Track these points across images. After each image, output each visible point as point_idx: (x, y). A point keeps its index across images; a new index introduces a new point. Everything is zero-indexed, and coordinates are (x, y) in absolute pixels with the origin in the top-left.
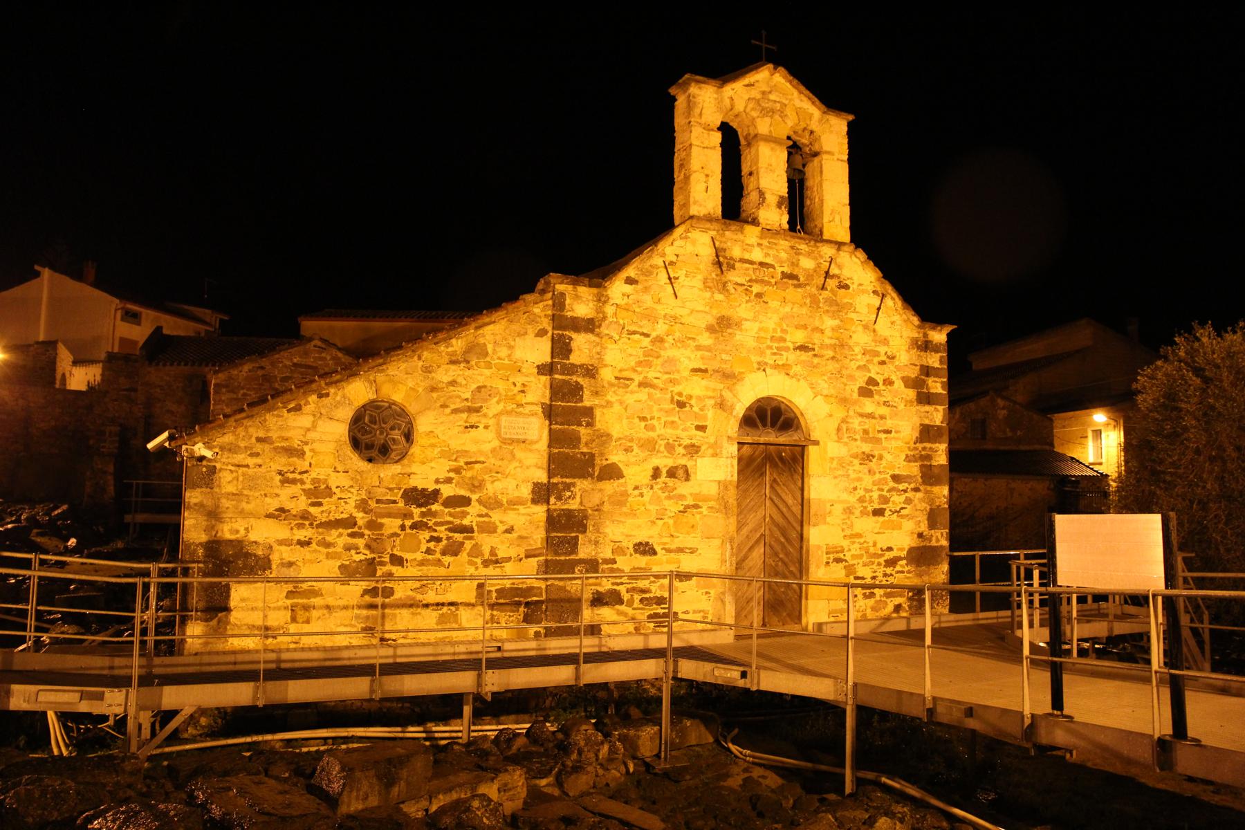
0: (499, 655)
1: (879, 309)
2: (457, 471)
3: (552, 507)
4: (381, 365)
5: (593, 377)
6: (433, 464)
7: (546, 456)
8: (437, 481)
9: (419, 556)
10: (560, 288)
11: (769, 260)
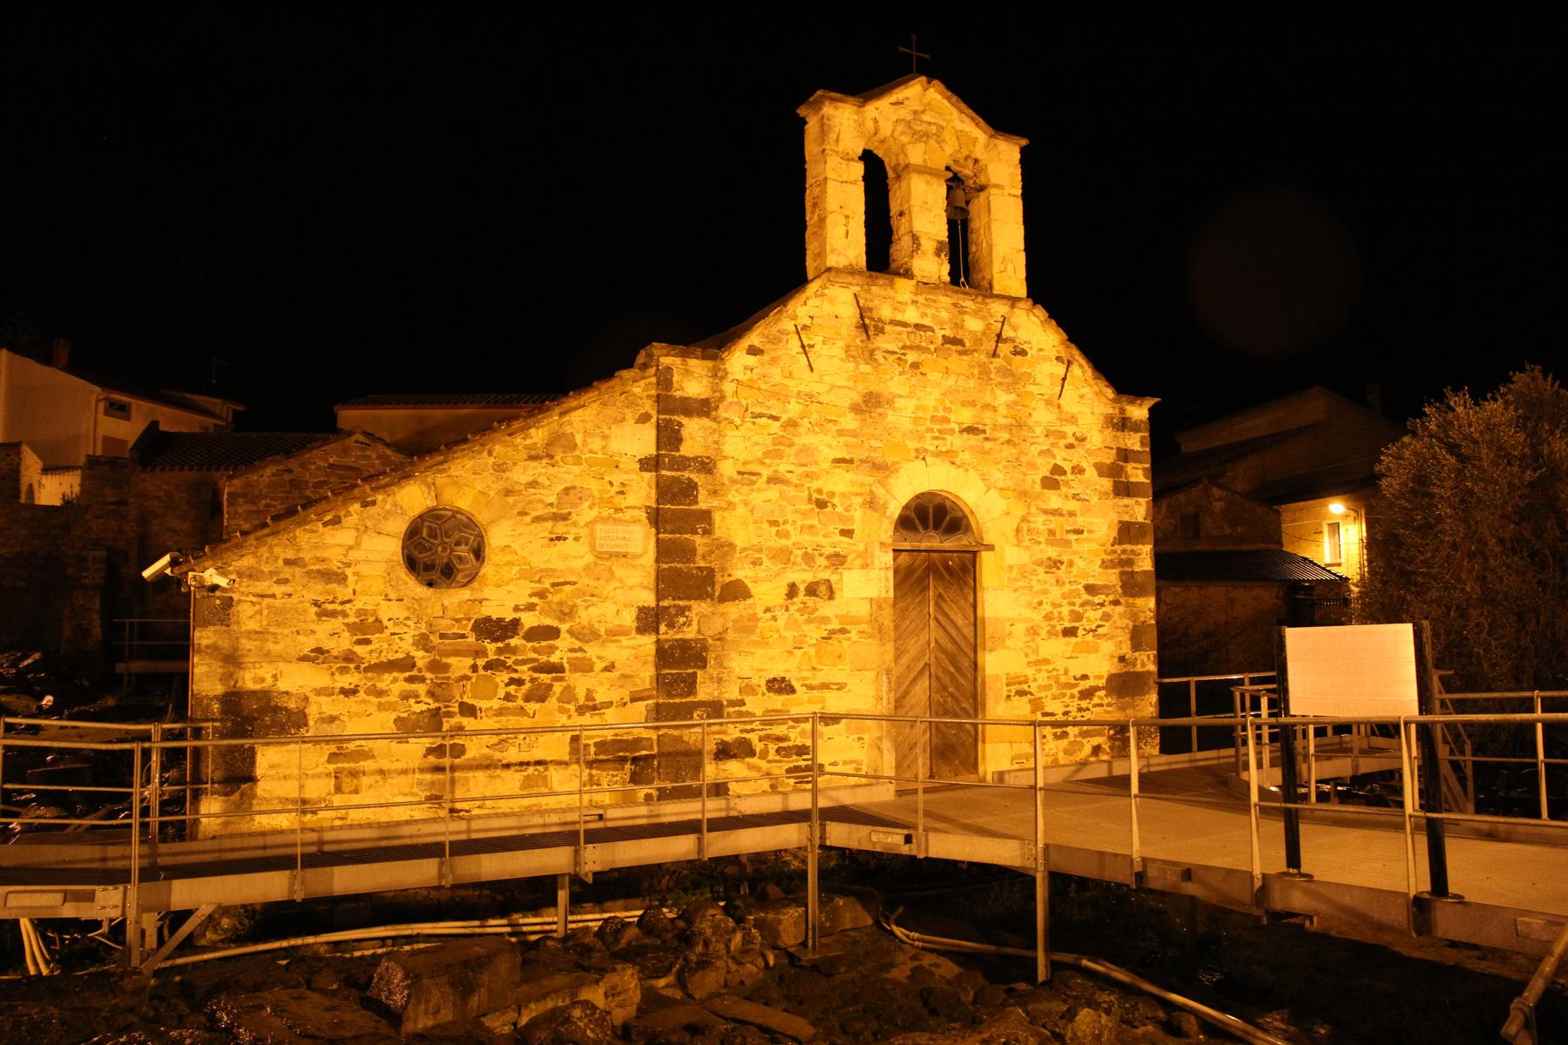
0: (600, 825)
1: (1064, 379)
3: (662, 637)
6: (510, 587)
8: (516, 609)
9: (496, 704)
10: (666, 361)
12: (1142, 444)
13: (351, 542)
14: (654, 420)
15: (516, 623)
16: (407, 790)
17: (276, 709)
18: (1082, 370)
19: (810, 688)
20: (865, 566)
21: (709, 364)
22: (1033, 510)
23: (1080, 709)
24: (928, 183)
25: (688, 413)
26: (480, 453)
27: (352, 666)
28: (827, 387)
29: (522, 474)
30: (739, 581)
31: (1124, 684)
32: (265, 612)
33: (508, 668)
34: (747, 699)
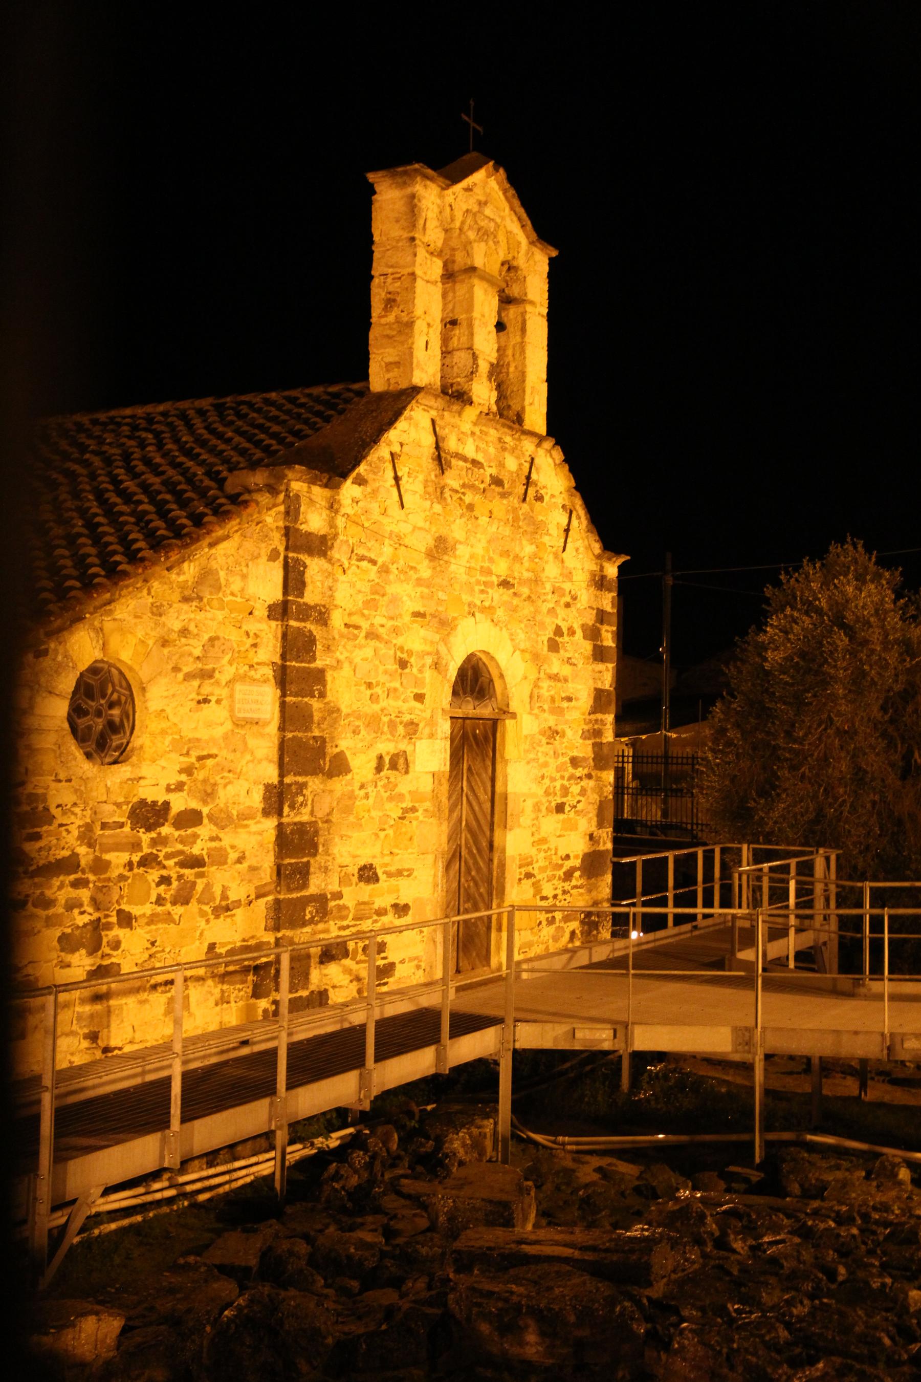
0: (245, 1051)
1: (567, 531)
2: (188, 771)
3: (285, 820)
4: (109, 602)
5: (325, 624)
6: (163, 763)
7: (276, 741)
8: (169, 789)
9: (147, 909)
10: (297, 486)
11: (480, 457)
12: (613, 607)
25: (311, 552)
28: (410, 528)
31: (591, 864)
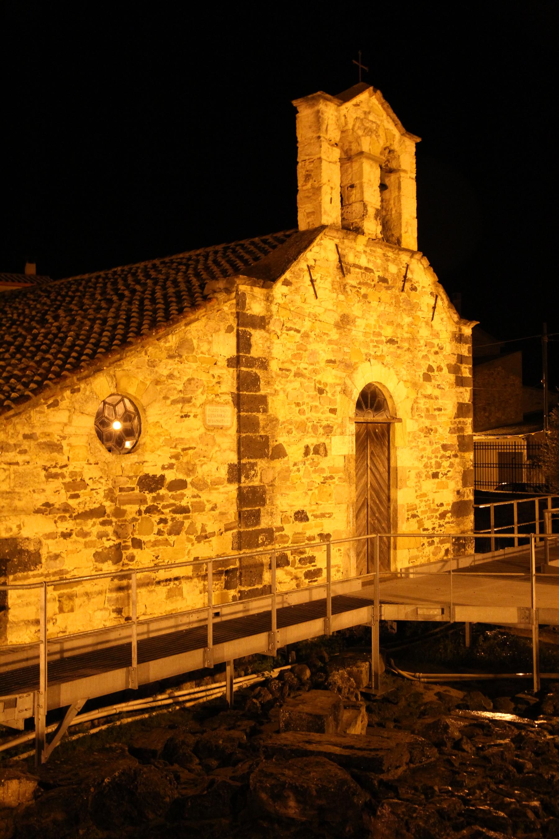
1: (434, 308)
3: (242, 485)
6: (159, 452)
8: (163, 468)
9: (152, 537)
13: (65, 420)
14: (235, 330)
15: (163, 477)
16: (101, 606)
17: (21, 552)
18: (443, 302)
19: (316, 516)
20: (342, 434)
21: (264, 291)
22: (419, 395)
23: (440, 526)
24: (371, 166)
25: (254, 326)
26: (140, 352)
27: (67, 515)
28: (323, 310)
29: (165, 368)
30: (281, 444)
31: (459, 509)
32: (12, 476)
33: (159, 511)
34: (286, 526)
